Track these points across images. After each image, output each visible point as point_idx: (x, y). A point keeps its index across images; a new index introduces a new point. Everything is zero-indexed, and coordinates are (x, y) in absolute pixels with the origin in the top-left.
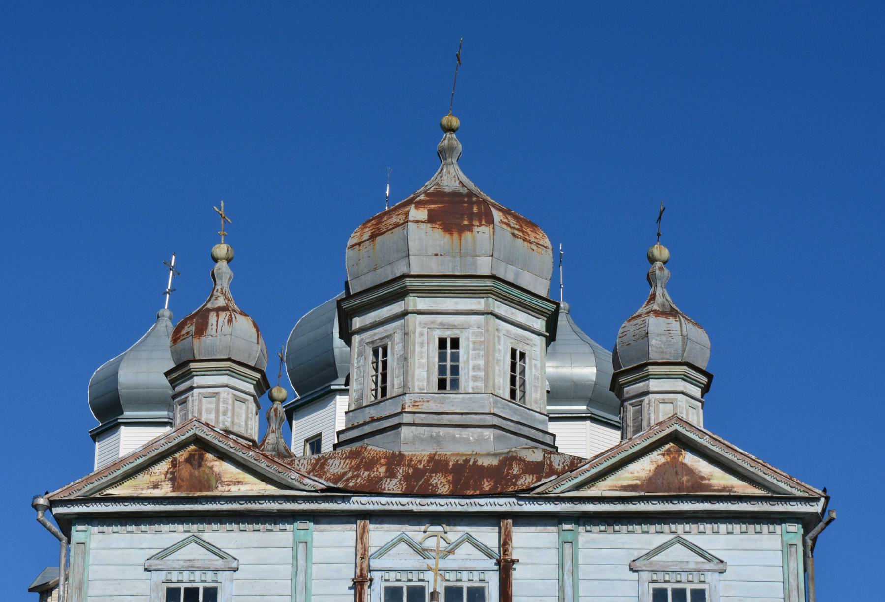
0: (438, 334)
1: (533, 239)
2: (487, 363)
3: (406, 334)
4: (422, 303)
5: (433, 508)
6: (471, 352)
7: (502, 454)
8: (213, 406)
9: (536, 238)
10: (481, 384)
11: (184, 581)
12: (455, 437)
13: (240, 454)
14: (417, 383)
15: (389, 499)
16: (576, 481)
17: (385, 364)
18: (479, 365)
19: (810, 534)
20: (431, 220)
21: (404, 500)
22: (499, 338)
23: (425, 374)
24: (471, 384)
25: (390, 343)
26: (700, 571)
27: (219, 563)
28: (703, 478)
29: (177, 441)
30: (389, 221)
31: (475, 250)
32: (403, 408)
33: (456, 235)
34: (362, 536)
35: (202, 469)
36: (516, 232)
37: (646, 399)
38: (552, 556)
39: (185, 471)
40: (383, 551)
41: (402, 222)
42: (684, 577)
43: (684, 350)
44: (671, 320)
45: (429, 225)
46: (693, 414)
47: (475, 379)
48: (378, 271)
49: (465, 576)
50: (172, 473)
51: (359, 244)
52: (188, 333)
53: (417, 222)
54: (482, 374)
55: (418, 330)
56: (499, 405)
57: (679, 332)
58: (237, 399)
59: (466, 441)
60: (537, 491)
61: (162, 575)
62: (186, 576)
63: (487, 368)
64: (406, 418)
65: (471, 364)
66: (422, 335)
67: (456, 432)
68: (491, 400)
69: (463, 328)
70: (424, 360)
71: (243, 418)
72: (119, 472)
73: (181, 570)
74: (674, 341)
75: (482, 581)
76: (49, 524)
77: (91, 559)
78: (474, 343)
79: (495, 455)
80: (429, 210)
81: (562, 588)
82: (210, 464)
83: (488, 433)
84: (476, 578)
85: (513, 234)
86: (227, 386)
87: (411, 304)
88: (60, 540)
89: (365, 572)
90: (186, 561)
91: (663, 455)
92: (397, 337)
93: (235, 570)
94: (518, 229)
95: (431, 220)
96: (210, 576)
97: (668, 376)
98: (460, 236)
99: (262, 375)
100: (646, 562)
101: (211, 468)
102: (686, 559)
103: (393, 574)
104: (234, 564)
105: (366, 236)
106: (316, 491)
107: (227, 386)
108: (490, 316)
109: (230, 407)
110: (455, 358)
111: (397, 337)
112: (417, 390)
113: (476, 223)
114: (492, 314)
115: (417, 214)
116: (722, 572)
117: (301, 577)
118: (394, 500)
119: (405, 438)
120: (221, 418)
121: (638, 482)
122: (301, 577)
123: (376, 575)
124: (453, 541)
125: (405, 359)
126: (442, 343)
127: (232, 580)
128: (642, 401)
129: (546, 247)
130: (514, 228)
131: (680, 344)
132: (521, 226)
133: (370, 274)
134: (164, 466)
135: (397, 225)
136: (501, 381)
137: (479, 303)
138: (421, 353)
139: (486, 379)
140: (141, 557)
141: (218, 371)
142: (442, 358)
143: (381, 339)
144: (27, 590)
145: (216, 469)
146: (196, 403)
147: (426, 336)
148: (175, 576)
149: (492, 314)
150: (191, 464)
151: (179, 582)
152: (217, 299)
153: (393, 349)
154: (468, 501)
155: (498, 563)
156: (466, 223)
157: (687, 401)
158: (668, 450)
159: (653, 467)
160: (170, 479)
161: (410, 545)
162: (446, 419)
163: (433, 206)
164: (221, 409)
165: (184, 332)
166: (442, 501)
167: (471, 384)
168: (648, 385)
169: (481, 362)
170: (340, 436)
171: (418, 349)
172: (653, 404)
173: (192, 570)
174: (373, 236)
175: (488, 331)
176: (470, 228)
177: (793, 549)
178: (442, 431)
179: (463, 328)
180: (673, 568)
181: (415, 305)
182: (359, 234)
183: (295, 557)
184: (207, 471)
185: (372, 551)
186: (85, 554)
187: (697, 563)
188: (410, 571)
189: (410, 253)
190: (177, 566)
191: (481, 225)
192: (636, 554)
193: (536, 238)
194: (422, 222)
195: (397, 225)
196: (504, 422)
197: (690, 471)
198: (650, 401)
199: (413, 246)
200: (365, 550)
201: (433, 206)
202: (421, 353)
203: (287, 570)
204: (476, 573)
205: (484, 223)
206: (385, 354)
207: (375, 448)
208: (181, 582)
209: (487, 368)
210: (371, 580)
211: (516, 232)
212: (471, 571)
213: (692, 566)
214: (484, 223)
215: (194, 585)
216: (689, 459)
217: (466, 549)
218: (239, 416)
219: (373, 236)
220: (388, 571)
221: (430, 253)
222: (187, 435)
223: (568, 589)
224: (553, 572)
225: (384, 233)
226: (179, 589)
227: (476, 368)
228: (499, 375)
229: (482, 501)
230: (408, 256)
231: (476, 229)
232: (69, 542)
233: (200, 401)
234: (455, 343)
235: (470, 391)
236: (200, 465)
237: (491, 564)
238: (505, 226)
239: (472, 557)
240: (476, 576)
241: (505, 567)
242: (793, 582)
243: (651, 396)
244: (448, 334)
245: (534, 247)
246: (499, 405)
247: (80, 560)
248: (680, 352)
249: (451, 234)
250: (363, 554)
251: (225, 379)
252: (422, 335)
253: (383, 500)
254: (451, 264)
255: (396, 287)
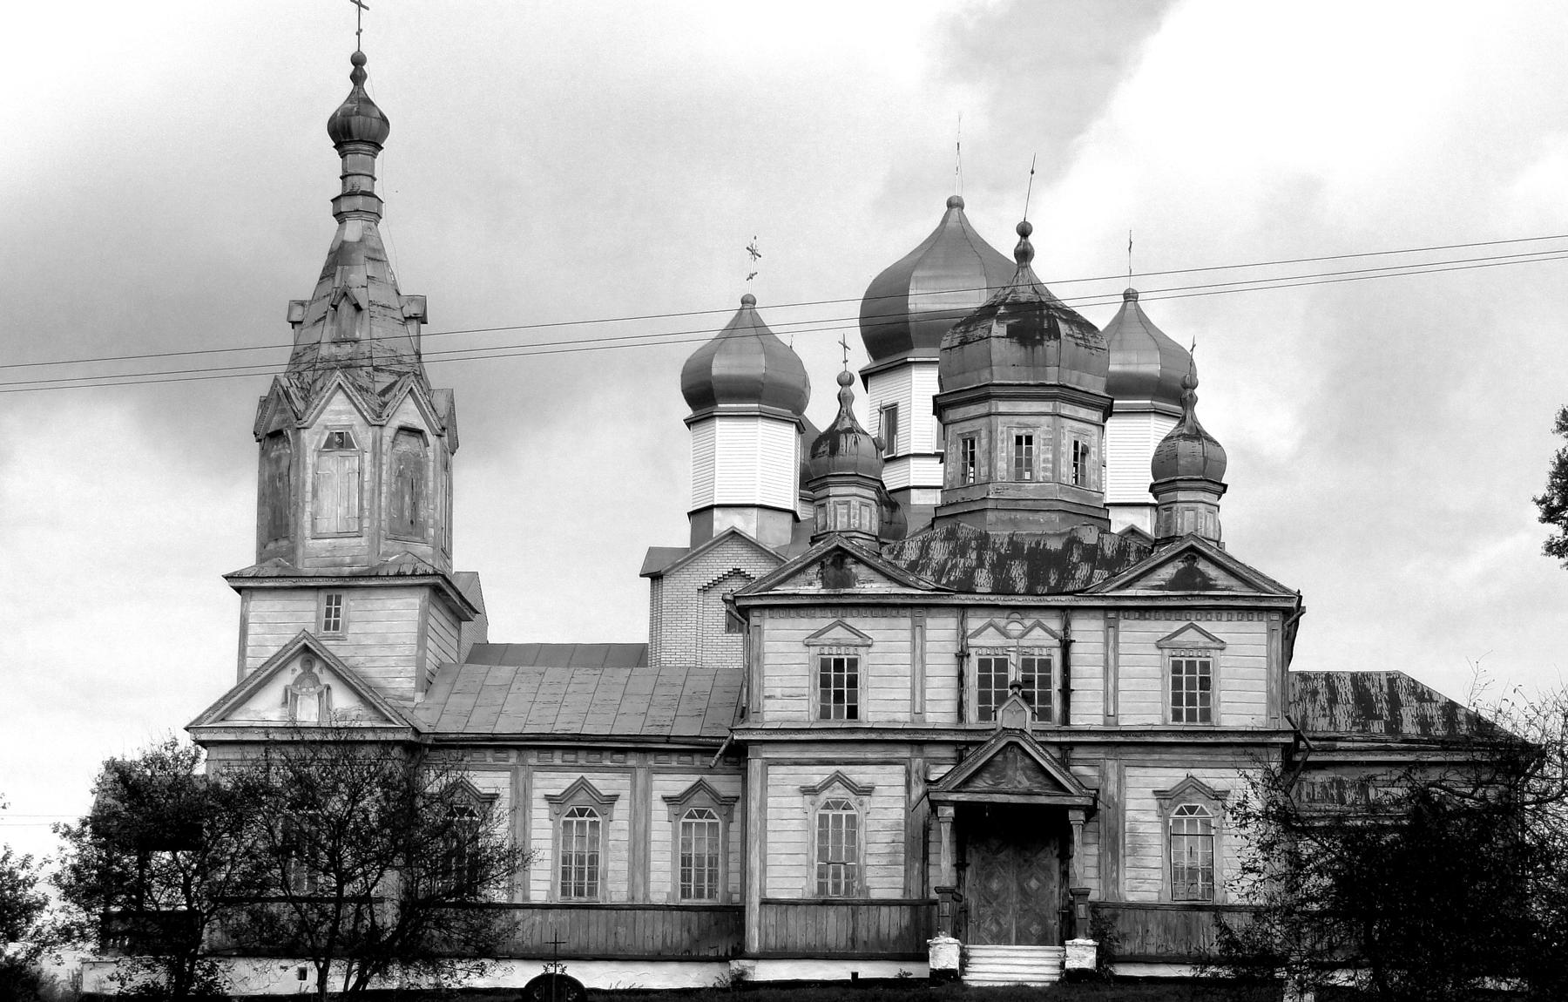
0: (1015, 432)
1: (1093, 344)
2: (1054, 455)
3: (991, 432)
4: (1003, 407)
5: (1013, 603)
6: (1042, 447)
7: (1064, 534)
8: (845, 511)
9: (1096, 342)
10: (1049, 474)
11: (834, 653)
12: (1029, 519)
13: (872, 561)
14: (999, 473)
15: (982, 597)
16: (1118, 583)
17: (972, 454)
18: (1048, 459)
19: (1287, 623)
20: (1010, 335)
21: (992, 597)
22: (1064, 433)
23: (1005, 465)
24: (1042, 474)
25: (976, 438)
26: (1208, 649)
27: (859, 641)
28: (1211, 579)
29: (824, 550)
30: (975, 332)
31: (1045, 362)
32: (988, 494)
33: (1029, 348)
34: (962, 622)
35: (843, 571)
36: (1079, 341)
37: (1175, 506)
38: (1100, 636)
39: (831, 571)
40: (978, 633)
41: (985, 336)
42: (1195, 653)
43: (1205, 468)
44: (1196, 443)
45: (1008, 339)
46: (1210, 517)
47: (1045, 469)
48: (967, 374)
49: (1036, 651)
50: (822, 574)
51: (950, 348)
52: (824, 452)
53: (998, 337)
54: (1050, 466)
55: (1000, 429)
56: (1064, 491)
57: (1201, 454)
58: (862, 504)
59: (1037, 522)
60: (1089, 591)
61: (817, 650)
62: (834, 650)
63: (1056, 461)
64: (990, 505)
65: (1042, 457)
66: (1002, 433)
67: (1031, 516)
68: (1057, 488)
69: (1035, 427)
70: (1004, 454)
71: (868, 519)
72: (783, 575)
73: (830, 646)
74: (1197, 461)
75: (1048, 655)
76: (734, 613)
77: (765, 637)
78: (1045, 439)
79: (1060, 535)
80: (1008, 326)
81: (1106, 661)
82: (849, 567)
83: (1055, 517)
84: (1045, 653)
85: (1077, 344)
86: (856, 495)
87: (993, 407)
88: (743, 624)
89: (964, 649)
90: (834, 639)
91: (1183, 562)
92: (984, 433)
93: (869, 646)
94: (1080, 339)
95: (1010, 335)
96: (852, 650)
97: (1191, 489)
98: (1033, 349)
99: (998, 932)
100: (1167, 642)
101: (850, 569)
102: (1196, 640)
103: (984, 650)
104: (869, 642)
105: (956, 343)
106: (929, 590)
107: (856, 495)
108: (1057, 417)
109: (858, 512)
110: (1029, 451)
111: (984, 433)
112: (999, 480)
113: (1046, 337)
114: (1058, 415)
115: (999, 329)
116: (1222, 649)
117: (918, 651)
118: (985, 597)
119: (990, 520)
120: (852, 521)
121: (1163, 583)
122: (918, 651)
123: (972, 651)
124: (1028, 625)
125: (990, 453)
126: (1019, 439)
127: (868, 653)
128: (1171, 508)
129: (1103, 349)
130: (1077, 338)
131: (1202, 464)
132: (1083, 335)
133: (959, 376)
134: (816, 569)
135: (981, 338)
136: (1066, 469)
137: (1048, 406)
138: (1002, 448)
139: (1053, 471)
140: (802, 635)
141: (849, 484)
142: (1019, 452)
143: (969, 433)
144: (854, 971)
145: (853, 570)
146: (832, 509)
147: (1005, 433)
148: (826, 650)
149: (1058, 415)
150: (835, 567)
151: (829, 654)
152: (843, 420)
153: (979, 442)
154: (1039, 598)
155: (1061, 641)
156: (1038, 337)
157: (1206, 509)
158: (1186, 558)
159: (1175, 571)
160: (820, 578)
161: (997, 629)
162: (1021, 505)
163: (1011, 322)
164: (852, 514)
165: (821, 450)
166: (1020, 598)
167: (1042, 474)
168: (1176, 495)
169: (1050, 456)
170: (938, 511)
171: (999, 445)
172: (1179, 510)
173: (839, 645)
174: (963, 343)
175: (1055, 429)
176: (1041, 342)
177: (1275, 633)
178: (1019, 515)
179: (1035, 427)
180: (1187, 647)
181: (997, 408)
182: (949, 338)
183: (914, 637)
184: (847, 572)
185: (970, 632)
186: (761, 634)
187: (1204, 643)
188: (997, 648)
189: (993, 364)
190: (828, 643)
191: (1050, 339)
192: (1161, 636)
193: (1096, 342)
194: (1003, 337)
195: (981, 338)
196: (1068, 505)
197: (1202, 574)
198: (1177, 508)
199: (995, 358)
200: (964, 632)
201: (1011, 322)
202: (1002, 448)
203: (907, 658)
204: (1045, 649)
205: (1052, 337)
206: (972, 446)
207: (967, 528)
208: (832, 654)
209: (1056, 461)
210: (969, 655)
211: (1079, 341)
212: (1040, 647)
213: (1201, 645)
214: (1052, 337)
215: (841, 657)
216: (1202, 565)
217: (1037, 632)
218: (865, 518)
219: (963, 343)
220: (981, 647)
221: (1008, 364)
222: (832, 546)
223: (1111, 662)
224: (1100, 648)
225: (971, 342)
226: (830, 659)
227: (1045, 461)
228: (1064, 465)
229: (1049, 598)
230: (991, 366)
231: (1046, 343)
232: (749, 624)
233: (835, 509)
234: (1029, 440)
235: (1041, 480)
236: (842, 568)
237: (1056, 642)
238: (1070, 338)
239: (1041, 637)
240: (1045, 652)
241: (1066, 646)
242: (1274, 657)
243: (1178, 504)
244: (1023, 432)
245: (1094, 352)
246: (1064, 491)
247: (757, 639)
248: (1202, 469)
249: (1026, 347)
250: (963, 635)
251: (854, 490)
252: (1002, 433)
253: (977, 597)
254: (1025, 374)
255: (982, 392)
